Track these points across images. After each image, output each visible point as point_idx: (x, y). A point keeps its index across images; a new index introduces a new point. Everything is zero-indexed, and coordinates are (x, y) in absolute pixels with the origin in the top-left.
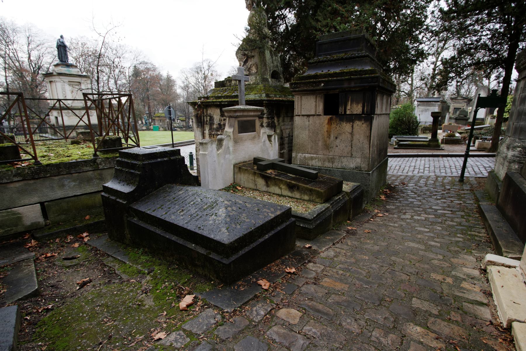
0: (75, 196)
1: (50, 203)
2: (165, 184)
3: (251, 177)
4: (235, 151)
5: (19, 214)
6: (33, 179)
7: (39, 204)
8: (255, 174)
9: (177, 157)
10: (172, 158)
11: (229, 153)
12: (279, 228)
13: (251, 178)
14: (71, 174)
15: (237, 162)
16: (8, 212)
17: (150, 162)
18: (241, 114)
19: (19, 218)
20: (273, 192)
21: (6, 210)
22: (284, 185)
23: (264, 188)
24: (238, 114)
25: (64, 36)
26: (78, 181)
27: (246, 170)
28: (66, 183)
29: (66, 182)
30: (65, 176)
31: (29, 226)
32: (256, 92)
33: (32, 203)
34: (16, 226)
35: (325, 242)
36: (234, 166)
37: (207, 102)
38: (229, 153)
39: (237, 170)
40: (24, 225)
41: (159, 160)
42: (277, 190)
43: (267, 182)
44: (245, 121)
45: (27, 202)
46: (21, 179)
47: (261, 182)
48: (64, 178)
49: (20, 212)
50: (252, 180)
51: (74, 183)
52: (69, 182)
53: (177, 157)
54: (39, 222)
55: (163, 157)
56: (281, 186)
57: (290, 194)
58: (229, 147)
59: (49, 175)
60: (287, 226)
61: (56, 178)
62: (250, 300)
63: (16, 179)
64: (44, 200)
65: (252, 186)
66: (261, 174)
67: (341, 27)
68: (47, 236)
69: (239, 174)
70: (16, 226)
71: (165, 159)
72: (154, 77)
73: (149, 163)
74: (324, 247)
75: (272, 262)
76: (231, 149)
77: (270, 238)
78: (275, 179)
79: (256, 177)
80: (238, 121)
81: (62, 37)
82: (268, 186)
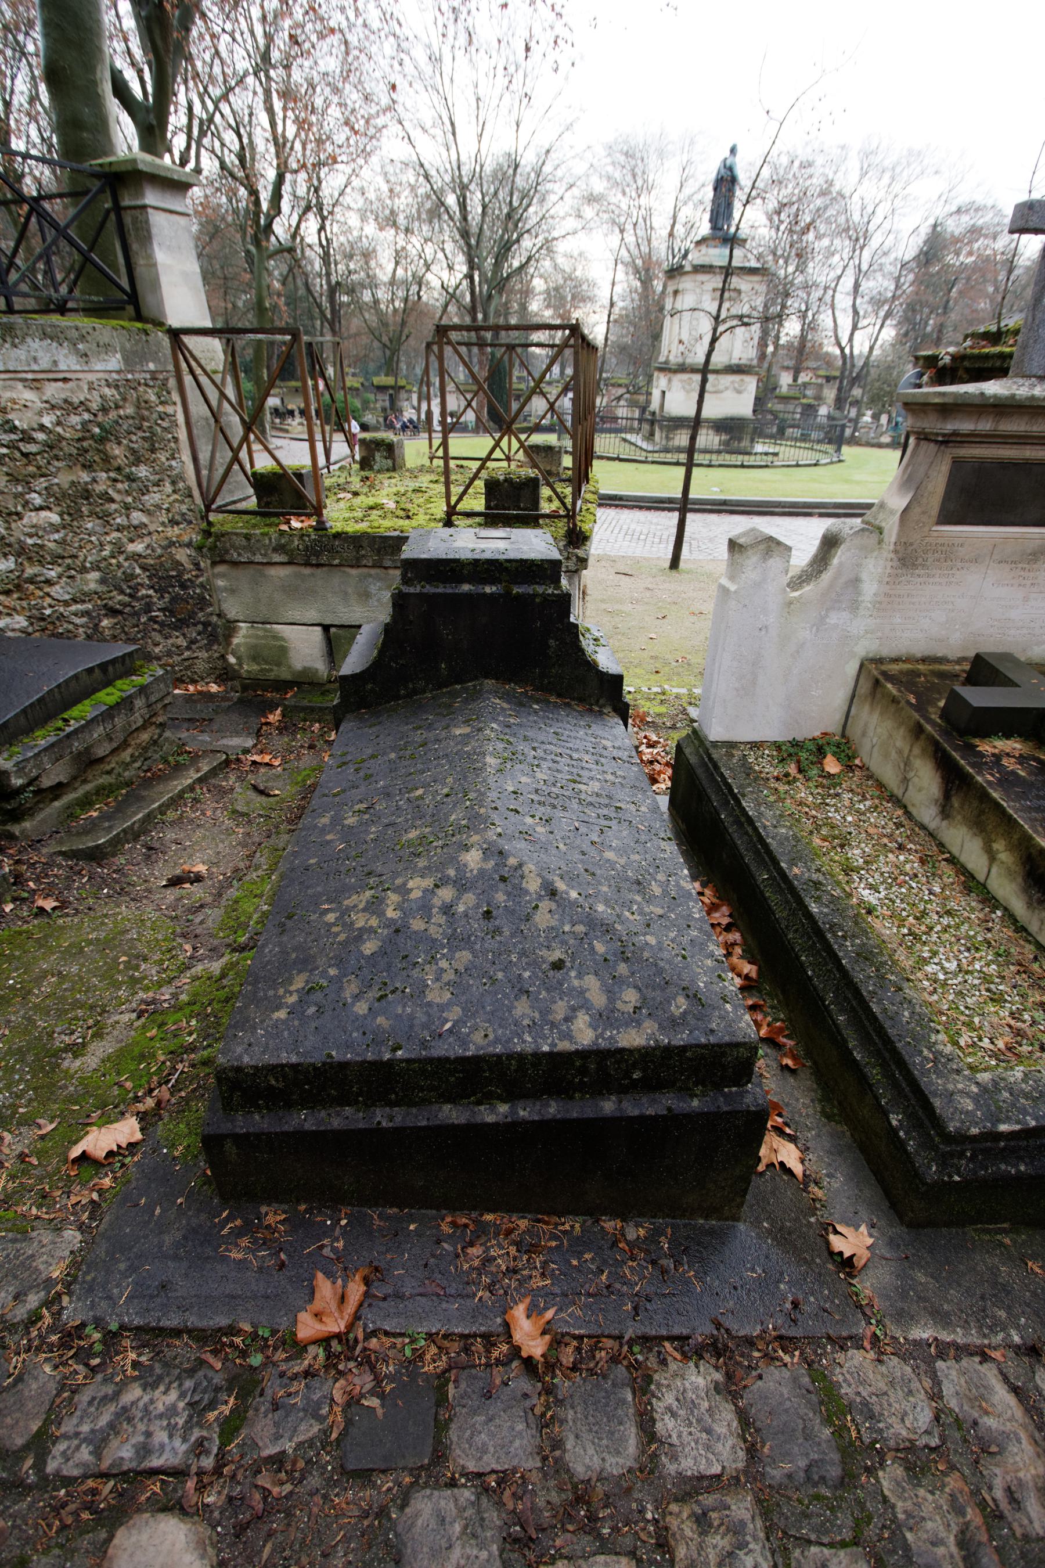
1: (341, 632)
2: (476, 678)
3: (900, 740)
4: (885, 603)
5: (283, 639)
6: (307, 564)
7: (319, 629)
8: (918, 731)
9: (540, 589)
10: (516, 590)
11: (854, 607)
12: (608, 1106)
13: (899, 744)
14: (386, 568)
15: (886, 652)
16: (266, 630)
17: (429, 589)
18: (985, 425)
19: (283, 651)
20: (955, 851)
22: (1010, 848)
23: (928, 815)
24: (966, 426)
25: (739, 149)
27: (894, 701)
28: (373, 589)
30: (373, 571)
34: (279, 664)
35: (1001, 1292)
36: (862, 666)
37: (987, 357)
38: (854, 607)
39: (865, 687)
41: (466, 587)
42: (970, 849)
43: (947, 796)
44: (1004, 465)
45: (297, 616)
46: (283, 558)
47: (925, 784)
48: (370, 576)
49: (285, 635)
50: (900, 752)
52: (380, 589)
53: (540, 589)
55: (485, 582)
56: (999, 846)
57: (1019, 906)
58: (856, 581)
59: (336, 562)
60: (672, 1118)
61: (354, 572)
62: (189, 1332)
63: (277, 558)
64: (327, 622)
65: (889, 775)
66: (936, 744)
68: (304, 709)
69: (867, 708)
70: (279, 664)
72: (987, 259)
73: (420, 595)
74: (942, 1318)
75: (522, 1210)
76: (870, 588)
77: (511, 1128)
78: (984, 796)
79: (916, 751)
80: (957, 463)
81: (733, 151)
82: (945, 812)
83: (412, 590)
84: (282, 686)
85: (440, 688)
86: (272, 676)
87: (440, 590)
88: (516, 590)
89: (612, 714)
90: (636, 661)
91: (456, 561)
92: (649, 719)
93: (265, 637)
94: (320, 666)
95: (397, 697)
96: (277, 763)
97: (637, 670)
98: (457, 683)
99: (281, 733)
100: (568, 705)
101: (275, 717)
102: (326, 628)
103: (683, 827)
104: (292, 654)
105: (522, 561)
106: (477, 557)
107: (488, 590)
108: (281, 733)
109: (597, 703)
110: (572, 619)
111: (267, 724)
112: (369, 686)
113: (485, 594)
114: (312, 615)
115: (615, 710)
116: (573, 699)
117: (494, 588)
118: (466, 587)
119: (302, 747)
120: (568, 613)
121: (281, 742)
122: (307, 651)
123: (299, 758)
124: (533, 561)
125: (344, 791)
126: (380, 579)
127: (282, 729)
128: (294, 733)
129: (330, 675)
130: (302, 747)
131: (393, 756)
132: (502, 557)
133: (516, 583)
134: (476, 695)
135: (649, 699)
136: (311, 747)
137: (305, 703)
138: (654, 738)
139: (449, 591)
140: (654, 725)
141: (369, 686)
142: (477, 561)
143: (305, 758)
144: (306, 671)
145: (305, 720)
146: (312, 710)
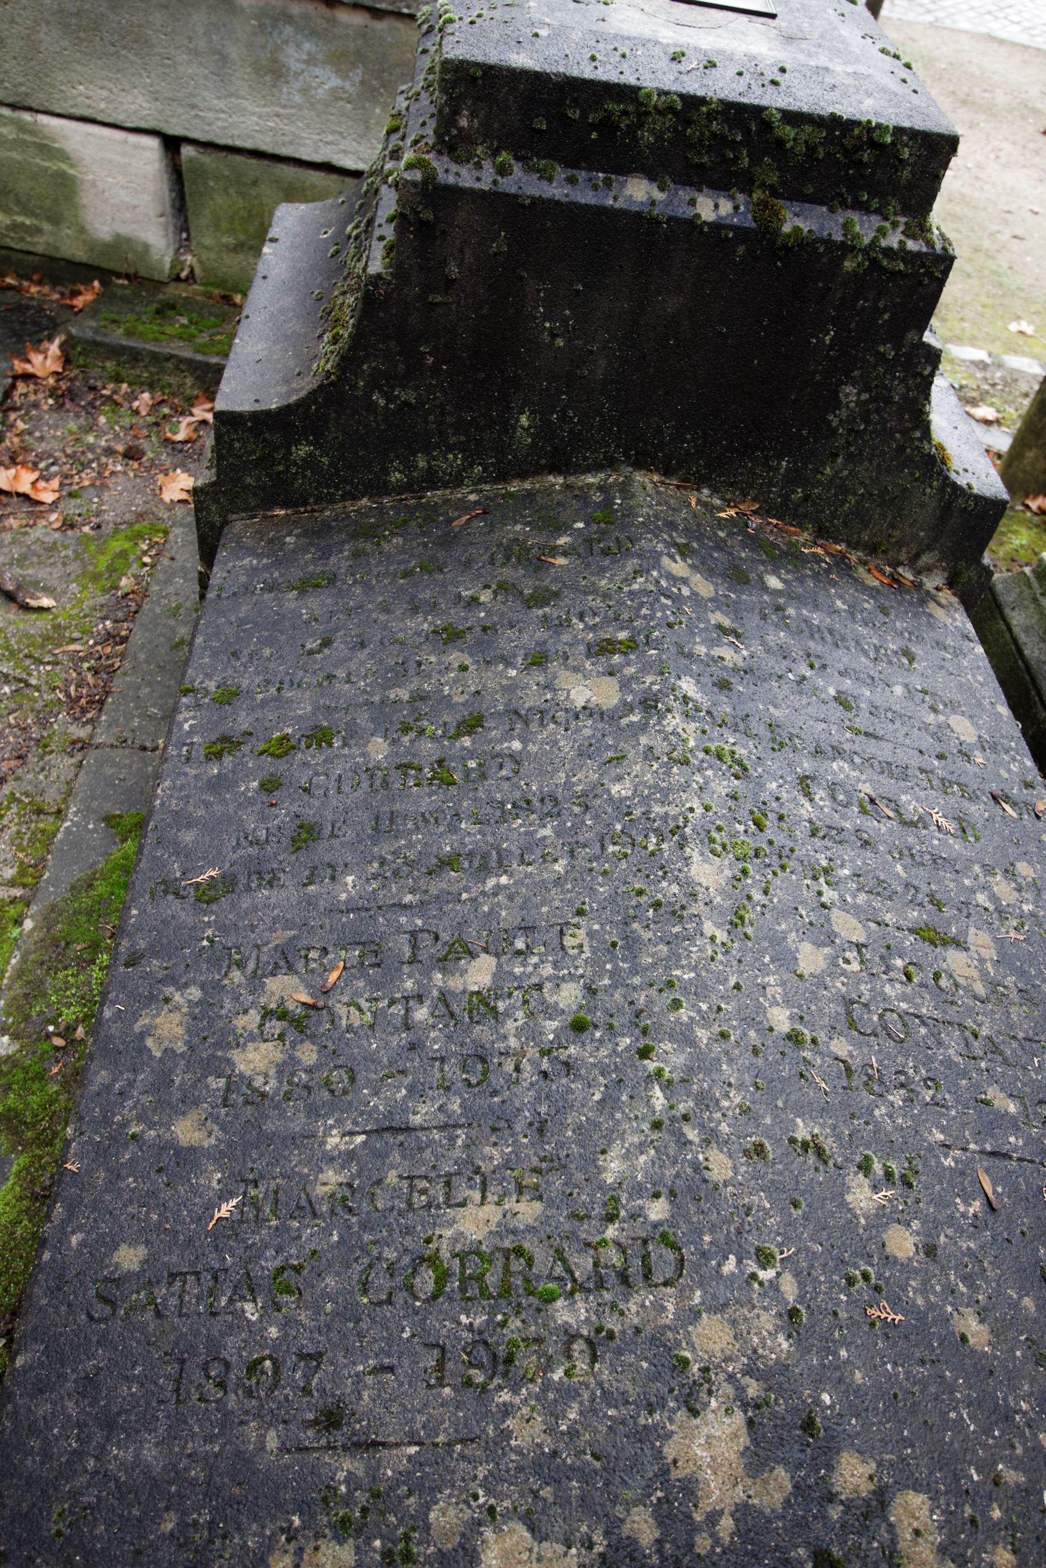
0: (327, 167)
1: (207, 159)
2: (610, 464)
5: (62, 155)
9: (865, 228)
10: (797, 221)
16: (21, 127)
17: (523, 182)
19: (62, 190)
21: (13, 107)
26: (357, 75)
28: (293, 57)
29: (291, 50)
31: (107, 246)
32: (697, 563)
33: (119, 118)
34: (56, 220)
40: (82, 230)
41: (638, 192)
51: (335, 82)
52: (311, 61)
53: (865, 228)
54: (147, 247)
67: (165, 516)
68: (115, 352)
70: (56, 220)
71: (710, 208)
83: (464, 177)
84: (67, 273)
85: (503, 477)
86: (39, 244)
87: (557, 190)
88: (797, 221)
89: (946, 596)
91: (626, 93)
93: (19, 144)
94: (156, 239)
95: (378, 488)
96: (48, 497)
98: (554, 469)
99: (59, 407)
100: (841, 562)
101: (45, 361)
102: (172, 144)
104: (86, 198)
105: (836, 126)
106: (693, 86)
108: (59, 407)
110: (928, 337)
111: (28, 377)
112: (303, 451)
113: (693, 224)
114: (136, 105)
117: (726, 207)
118: (638, 192)
119: (109, 452)
120: (923, 324)
121: (56, 430)
122: (124, 196)
123: (100, 485)
124: (869, 128)
125: (228, 883)
126: (314, 34)
127: (64, 397)
128: (91, 409)
129: (176, 263)
130: (109, 452)
131: (379, 749)
132: (774, 100)
133: (796, 196)
134: (610, 537)
136: (132, 454)
137: (117, 336)
139: (586, 197)
141: (303, 451)
142: (693, 102)
143: (117, 485)
144: (120, 244)
145: (118, 379)
146: (135, 356)
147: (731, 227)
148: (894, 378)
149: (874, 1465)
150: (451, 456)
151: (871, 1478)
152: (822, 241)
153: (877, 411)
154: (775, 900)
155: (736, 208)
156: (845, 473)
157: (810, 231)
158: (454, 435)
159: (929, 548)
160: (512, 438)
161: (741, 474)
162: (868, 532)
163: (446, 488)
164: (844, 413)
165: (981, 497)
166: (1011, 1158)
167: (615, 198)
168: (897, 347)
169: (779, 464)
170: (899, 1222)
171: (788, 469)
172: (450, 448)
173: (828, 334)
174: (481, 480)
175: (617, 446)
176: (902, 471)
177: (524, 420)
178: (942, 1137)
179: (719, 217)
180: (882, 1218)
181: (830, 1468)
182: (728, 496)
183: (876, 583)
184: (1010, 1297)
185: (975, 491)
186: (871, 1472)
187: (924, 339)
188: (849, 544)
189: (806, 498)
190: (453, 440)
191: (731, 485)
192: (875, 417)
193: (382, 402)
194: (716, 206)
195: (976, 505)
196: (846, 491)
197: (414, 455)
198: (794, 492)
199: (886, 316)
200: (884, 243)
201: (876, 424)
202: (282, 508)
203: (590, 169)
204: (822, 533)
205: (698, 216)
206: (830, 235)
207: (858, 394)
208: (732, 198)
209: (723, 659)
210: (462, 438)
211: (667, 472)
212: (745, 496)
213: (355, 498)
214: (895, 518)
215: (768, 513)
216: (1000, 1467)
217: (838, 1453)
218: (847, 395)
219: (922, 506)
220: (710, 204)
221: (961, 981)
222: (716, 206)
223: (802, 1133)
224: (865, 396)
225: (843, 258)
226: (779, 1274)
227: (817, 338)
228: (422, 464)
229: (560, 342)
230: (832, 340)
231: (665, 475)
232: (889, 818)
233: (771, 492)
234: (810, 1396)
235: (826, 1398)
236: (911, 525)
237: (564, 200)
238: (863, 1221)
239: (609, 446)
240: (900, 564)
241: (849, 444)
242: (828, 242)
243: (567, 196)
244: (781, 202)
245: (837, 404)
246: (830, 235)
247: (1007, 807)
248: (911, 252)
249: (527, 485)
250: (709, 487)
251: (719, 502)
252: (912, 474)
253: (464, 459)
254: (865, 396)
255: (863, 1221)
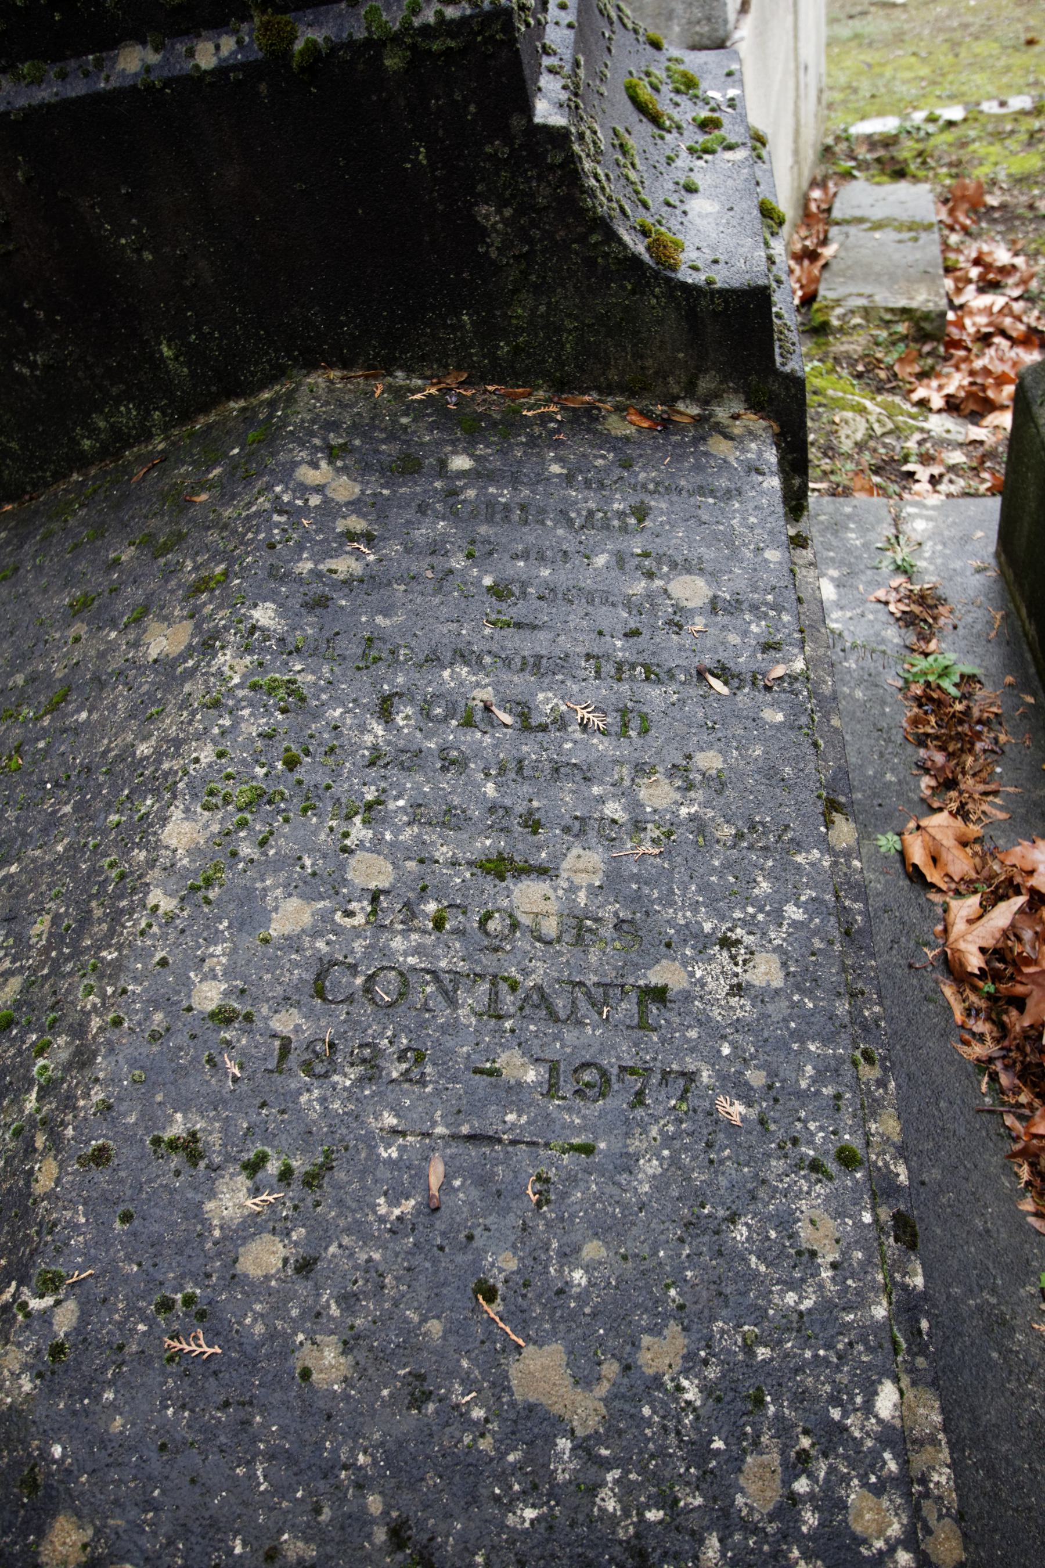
2: (278, 374)
41: (133, 61)
85: (186, 416)
87: (44, 94)
90: (979, 20)
92: (992, 200)
97: (980, 48)
100: (585, 420)
103: (1031, 629)
107: (206, 56)
109: (690, 392)
113: (197, 79)
115: (755, 406)
116: (607, 390)
117: (228, 44)
118: (133, 61)
135: (999, 137)
138: (1002, 256)
139: (77, 88)
140: (1007, 218)
147: (235, 68)
148: (528, 180)
149: (90, 1532)
150: (122, 408)
151: (85, 1546)
152: (342, 46)
153: (533, 224)
154: (272, 852)
155: (239, 42)
156: (543, 308)
157: (327, 39)
158: (112, 385)
159: (701, 370)
160: (168, 372)
161: (426, 344)
162: (613, 371)
163: (140, 443)
164: (496, 240)
165: (727, 291)
166: (500, 1141)
167: (107, 79)
168: (508, 140)
169: (460, 320)
170: (274, 1231)
171: (473, 323)
172: (118, 401)
173: (420, 153)
174: (166, 428)
175: (276, 351)
176: (608, 287)
177: (166, 351)
178: (395, 1121)
179: (225, 60)
180: (252, 1226)
181: (41, 1533)
182: (428, 373)
183: (630, 430)
184: (407, 1321)
185: (718, 286)
186: (86, 1540)
187: (538, 120)
188: (600, 392)
189: (517, 350)
190: (114, 391)
191: (423, 358)
192: (536, 233)
193: (26, 371)
194: (218, 48)
195: (726, 301)
196: (558, 329)
197: (90, 417)
198: (498, 347)
199: (472, 108)
200: (417, 22)
201: (541, 240)
202: (8, 503)
203: (78, 55)
204: (561, 386)
205: (197, 67)
206: (350, 35)
207: (499, 212)
208: (235, 32)
209: (335, 572)
210: (122, 387)
211: (346, 364)
212: (446, 366)
213: (66, 476)
214: (635, 345)
215: (484, 380)
216: (286, 1536)
217: (54, 1517)
218: (487, 217)
219: (660, 322)
220: (210, 46)
221: (525, 920)
222: (218, 48)
223: (177, 1127)
224: (508, 212)
225: (379, 58)
226: (58, 1303)
227: (410, 161)
228: (102, 424)
229: (148, 256)
230: (427, 157)
231: (344, 367)
232: (506, 726)
233: (472, 355)
234: (38, 1448)
235: (57, 1451)
236: (660, 348)
237: (53, 100)
238: (217, 1233)
239: (267, 353)
240: (676, 398)
241: (525, 274)
242: (350, 44)
243: (57, 94)
244: (288, 17)
245: (483, 233)
246: (350, 35)
247: (713, 681)
248: (452, 21)
249: (212, 418)
250: (400, 368)
251: (420, 382)
252: (623, 288)
253: (137, 408)
254: (508, 212)
255: (217, 1233)
